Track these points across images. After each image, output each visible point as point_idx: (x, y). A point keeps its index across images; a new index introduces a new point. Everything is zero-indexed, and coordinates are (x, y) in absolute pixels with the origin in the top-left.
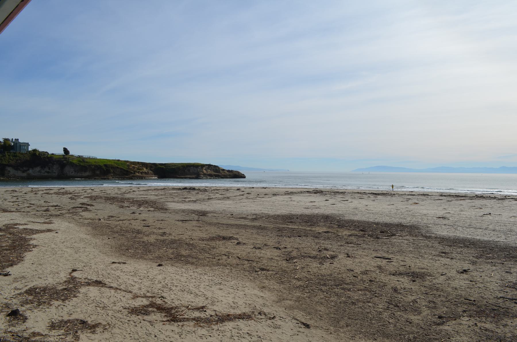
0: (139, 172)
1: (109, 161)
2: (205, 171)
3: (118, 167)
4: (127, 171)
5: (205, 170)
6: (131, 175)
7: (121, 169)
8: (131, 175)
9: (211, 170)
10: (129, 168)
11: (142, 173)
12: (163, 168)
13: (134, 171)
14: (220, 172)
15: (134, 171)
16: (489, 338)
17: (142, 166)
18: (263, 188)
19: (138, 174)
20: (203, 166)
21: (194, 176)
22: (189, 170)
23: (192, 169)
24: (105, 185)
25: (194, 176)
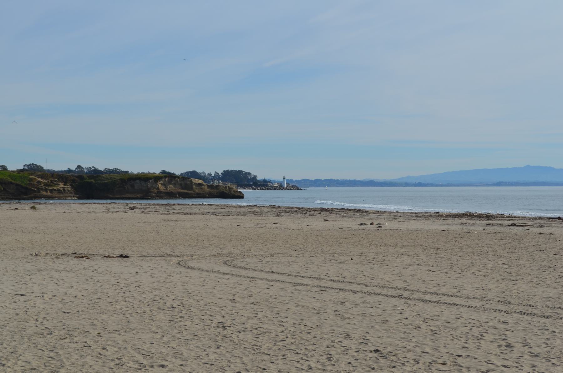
0: (46, 190)
1: (62, 171)
2: (161, 187)
3: (11, 183)
4: (26, 188)
5: (163, 184)
6: (33, 195)
7: (17, 185)
8: (33, 195)
9: (175, 184)
10: (30, 184)
11: (51, 191)
12: (91, 183)
13: (38, 189)
14: (191, 189)
15: (38, 189)
16: (52, 372)
17: (59, 181)
18: (550, 218)
19: (44, 193)
20: (156, 178)
21: (138, 196)
22: (133, 186)
23: (137, 185)
24: (393, 208)
25: (138, 196)
